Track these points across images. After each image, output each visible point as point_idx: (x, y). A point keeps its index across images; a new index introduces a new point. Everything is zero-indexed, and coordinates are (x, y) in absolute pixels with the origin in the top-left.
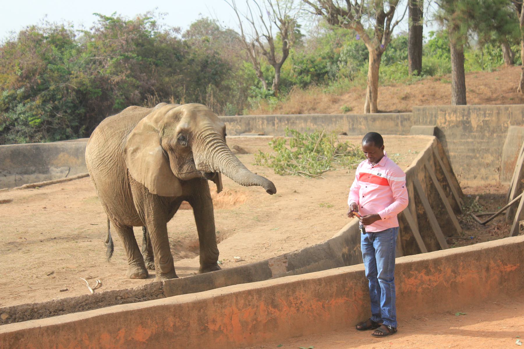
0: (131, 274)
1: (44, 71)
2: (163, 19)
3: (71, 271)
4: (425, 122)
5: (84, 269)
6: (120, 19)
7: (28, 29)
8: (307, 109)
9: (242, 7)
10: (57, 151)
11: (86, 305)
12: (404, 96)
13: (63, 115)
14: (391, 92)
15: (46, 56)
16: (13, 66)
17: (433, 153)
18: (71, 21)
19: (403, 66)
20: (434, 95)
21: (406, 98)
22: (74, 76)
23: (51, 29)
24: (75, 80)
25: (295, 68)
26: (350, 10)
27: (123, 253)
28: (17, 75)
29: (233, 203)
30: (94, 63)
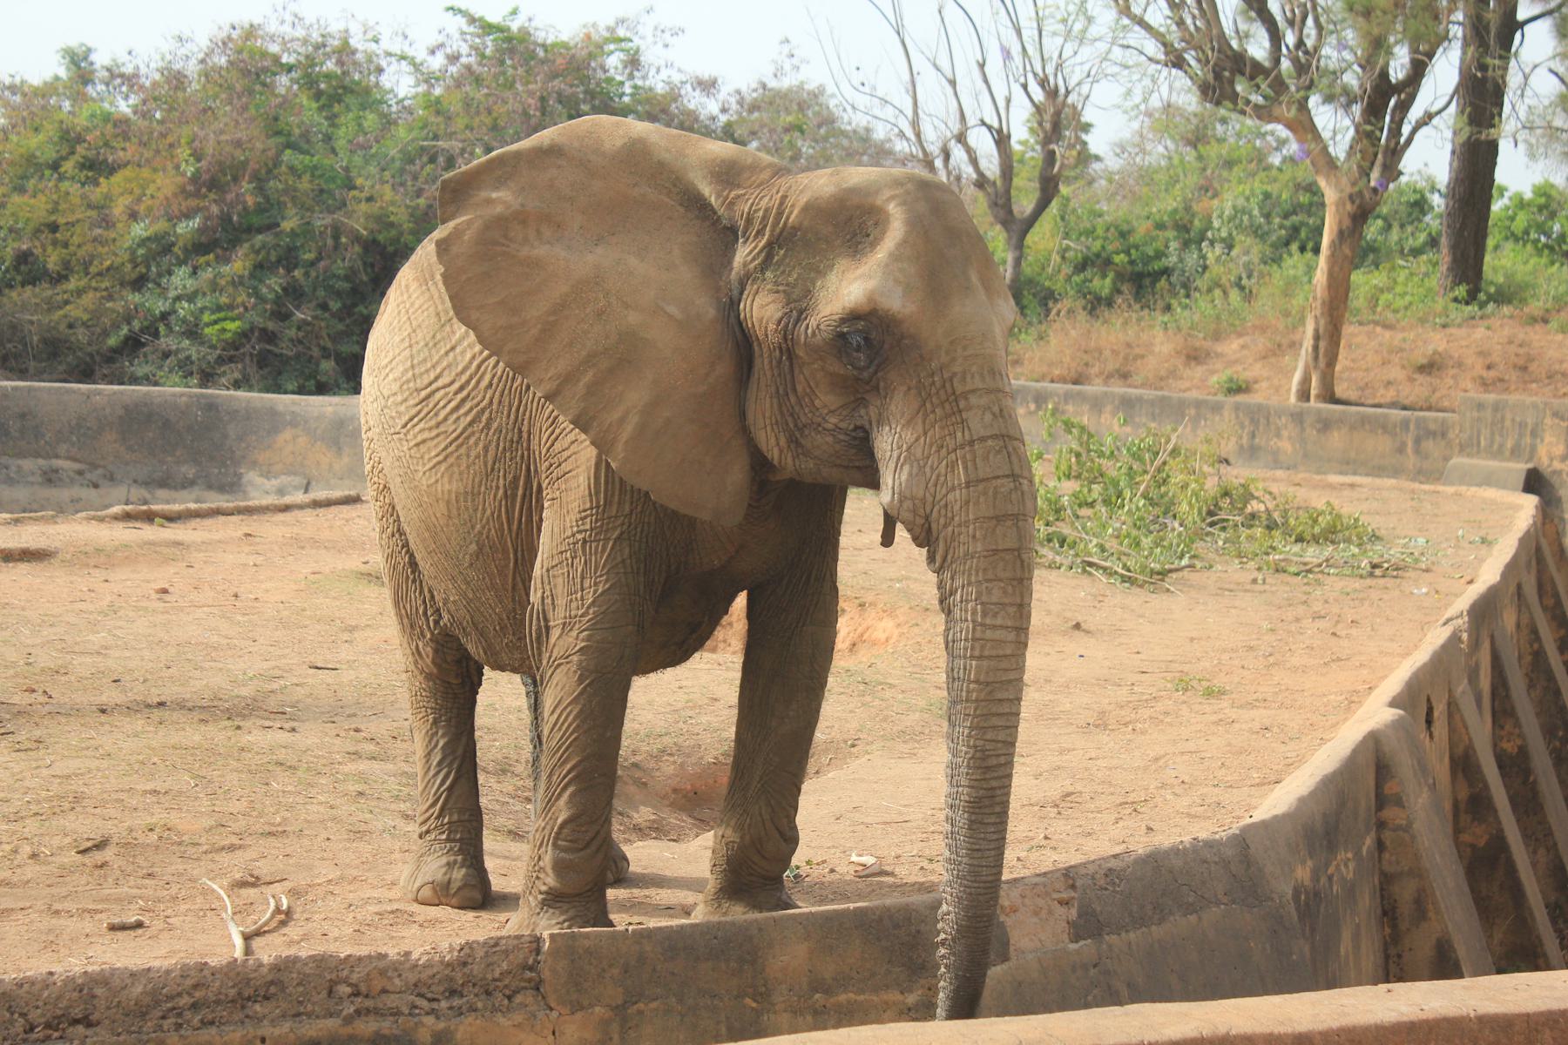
0: (417, 885)
1: (269, 171)
2: (666, 46)
3: (180, 844)
4: (1496, 447)
5: (234, 840)
6: (529, 34)
7: (235, 35)
8: (1101, 373)
9: (922, 27)
10: (275, 421)
11: (194, 1006)
12: (1424, 361)
13: (315, 317)
14: (1381, 345)
15: (281, 125)
16: (171, 146)
17: (1538, 549)
18: (371, 23)
19: (1412, 274)
20: (1524, 369)
21: (1430, 367)
22: (363, 195)
23: (305, 42)
24: (364, 207)
25: (1068, 249)
26: (1277, 61)
27: (406, 790)
28: (183, 174)
29: (847, 644)
30: (432, 160)
